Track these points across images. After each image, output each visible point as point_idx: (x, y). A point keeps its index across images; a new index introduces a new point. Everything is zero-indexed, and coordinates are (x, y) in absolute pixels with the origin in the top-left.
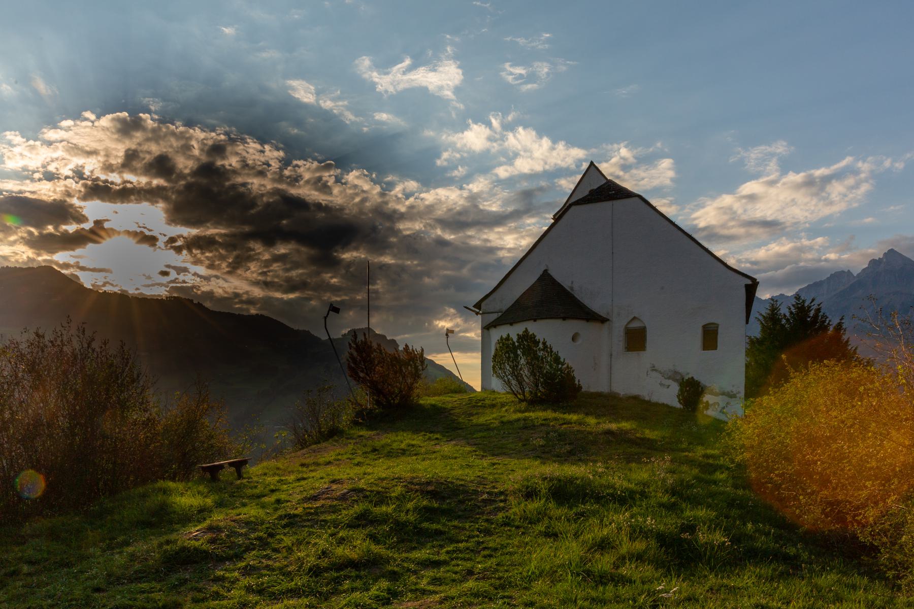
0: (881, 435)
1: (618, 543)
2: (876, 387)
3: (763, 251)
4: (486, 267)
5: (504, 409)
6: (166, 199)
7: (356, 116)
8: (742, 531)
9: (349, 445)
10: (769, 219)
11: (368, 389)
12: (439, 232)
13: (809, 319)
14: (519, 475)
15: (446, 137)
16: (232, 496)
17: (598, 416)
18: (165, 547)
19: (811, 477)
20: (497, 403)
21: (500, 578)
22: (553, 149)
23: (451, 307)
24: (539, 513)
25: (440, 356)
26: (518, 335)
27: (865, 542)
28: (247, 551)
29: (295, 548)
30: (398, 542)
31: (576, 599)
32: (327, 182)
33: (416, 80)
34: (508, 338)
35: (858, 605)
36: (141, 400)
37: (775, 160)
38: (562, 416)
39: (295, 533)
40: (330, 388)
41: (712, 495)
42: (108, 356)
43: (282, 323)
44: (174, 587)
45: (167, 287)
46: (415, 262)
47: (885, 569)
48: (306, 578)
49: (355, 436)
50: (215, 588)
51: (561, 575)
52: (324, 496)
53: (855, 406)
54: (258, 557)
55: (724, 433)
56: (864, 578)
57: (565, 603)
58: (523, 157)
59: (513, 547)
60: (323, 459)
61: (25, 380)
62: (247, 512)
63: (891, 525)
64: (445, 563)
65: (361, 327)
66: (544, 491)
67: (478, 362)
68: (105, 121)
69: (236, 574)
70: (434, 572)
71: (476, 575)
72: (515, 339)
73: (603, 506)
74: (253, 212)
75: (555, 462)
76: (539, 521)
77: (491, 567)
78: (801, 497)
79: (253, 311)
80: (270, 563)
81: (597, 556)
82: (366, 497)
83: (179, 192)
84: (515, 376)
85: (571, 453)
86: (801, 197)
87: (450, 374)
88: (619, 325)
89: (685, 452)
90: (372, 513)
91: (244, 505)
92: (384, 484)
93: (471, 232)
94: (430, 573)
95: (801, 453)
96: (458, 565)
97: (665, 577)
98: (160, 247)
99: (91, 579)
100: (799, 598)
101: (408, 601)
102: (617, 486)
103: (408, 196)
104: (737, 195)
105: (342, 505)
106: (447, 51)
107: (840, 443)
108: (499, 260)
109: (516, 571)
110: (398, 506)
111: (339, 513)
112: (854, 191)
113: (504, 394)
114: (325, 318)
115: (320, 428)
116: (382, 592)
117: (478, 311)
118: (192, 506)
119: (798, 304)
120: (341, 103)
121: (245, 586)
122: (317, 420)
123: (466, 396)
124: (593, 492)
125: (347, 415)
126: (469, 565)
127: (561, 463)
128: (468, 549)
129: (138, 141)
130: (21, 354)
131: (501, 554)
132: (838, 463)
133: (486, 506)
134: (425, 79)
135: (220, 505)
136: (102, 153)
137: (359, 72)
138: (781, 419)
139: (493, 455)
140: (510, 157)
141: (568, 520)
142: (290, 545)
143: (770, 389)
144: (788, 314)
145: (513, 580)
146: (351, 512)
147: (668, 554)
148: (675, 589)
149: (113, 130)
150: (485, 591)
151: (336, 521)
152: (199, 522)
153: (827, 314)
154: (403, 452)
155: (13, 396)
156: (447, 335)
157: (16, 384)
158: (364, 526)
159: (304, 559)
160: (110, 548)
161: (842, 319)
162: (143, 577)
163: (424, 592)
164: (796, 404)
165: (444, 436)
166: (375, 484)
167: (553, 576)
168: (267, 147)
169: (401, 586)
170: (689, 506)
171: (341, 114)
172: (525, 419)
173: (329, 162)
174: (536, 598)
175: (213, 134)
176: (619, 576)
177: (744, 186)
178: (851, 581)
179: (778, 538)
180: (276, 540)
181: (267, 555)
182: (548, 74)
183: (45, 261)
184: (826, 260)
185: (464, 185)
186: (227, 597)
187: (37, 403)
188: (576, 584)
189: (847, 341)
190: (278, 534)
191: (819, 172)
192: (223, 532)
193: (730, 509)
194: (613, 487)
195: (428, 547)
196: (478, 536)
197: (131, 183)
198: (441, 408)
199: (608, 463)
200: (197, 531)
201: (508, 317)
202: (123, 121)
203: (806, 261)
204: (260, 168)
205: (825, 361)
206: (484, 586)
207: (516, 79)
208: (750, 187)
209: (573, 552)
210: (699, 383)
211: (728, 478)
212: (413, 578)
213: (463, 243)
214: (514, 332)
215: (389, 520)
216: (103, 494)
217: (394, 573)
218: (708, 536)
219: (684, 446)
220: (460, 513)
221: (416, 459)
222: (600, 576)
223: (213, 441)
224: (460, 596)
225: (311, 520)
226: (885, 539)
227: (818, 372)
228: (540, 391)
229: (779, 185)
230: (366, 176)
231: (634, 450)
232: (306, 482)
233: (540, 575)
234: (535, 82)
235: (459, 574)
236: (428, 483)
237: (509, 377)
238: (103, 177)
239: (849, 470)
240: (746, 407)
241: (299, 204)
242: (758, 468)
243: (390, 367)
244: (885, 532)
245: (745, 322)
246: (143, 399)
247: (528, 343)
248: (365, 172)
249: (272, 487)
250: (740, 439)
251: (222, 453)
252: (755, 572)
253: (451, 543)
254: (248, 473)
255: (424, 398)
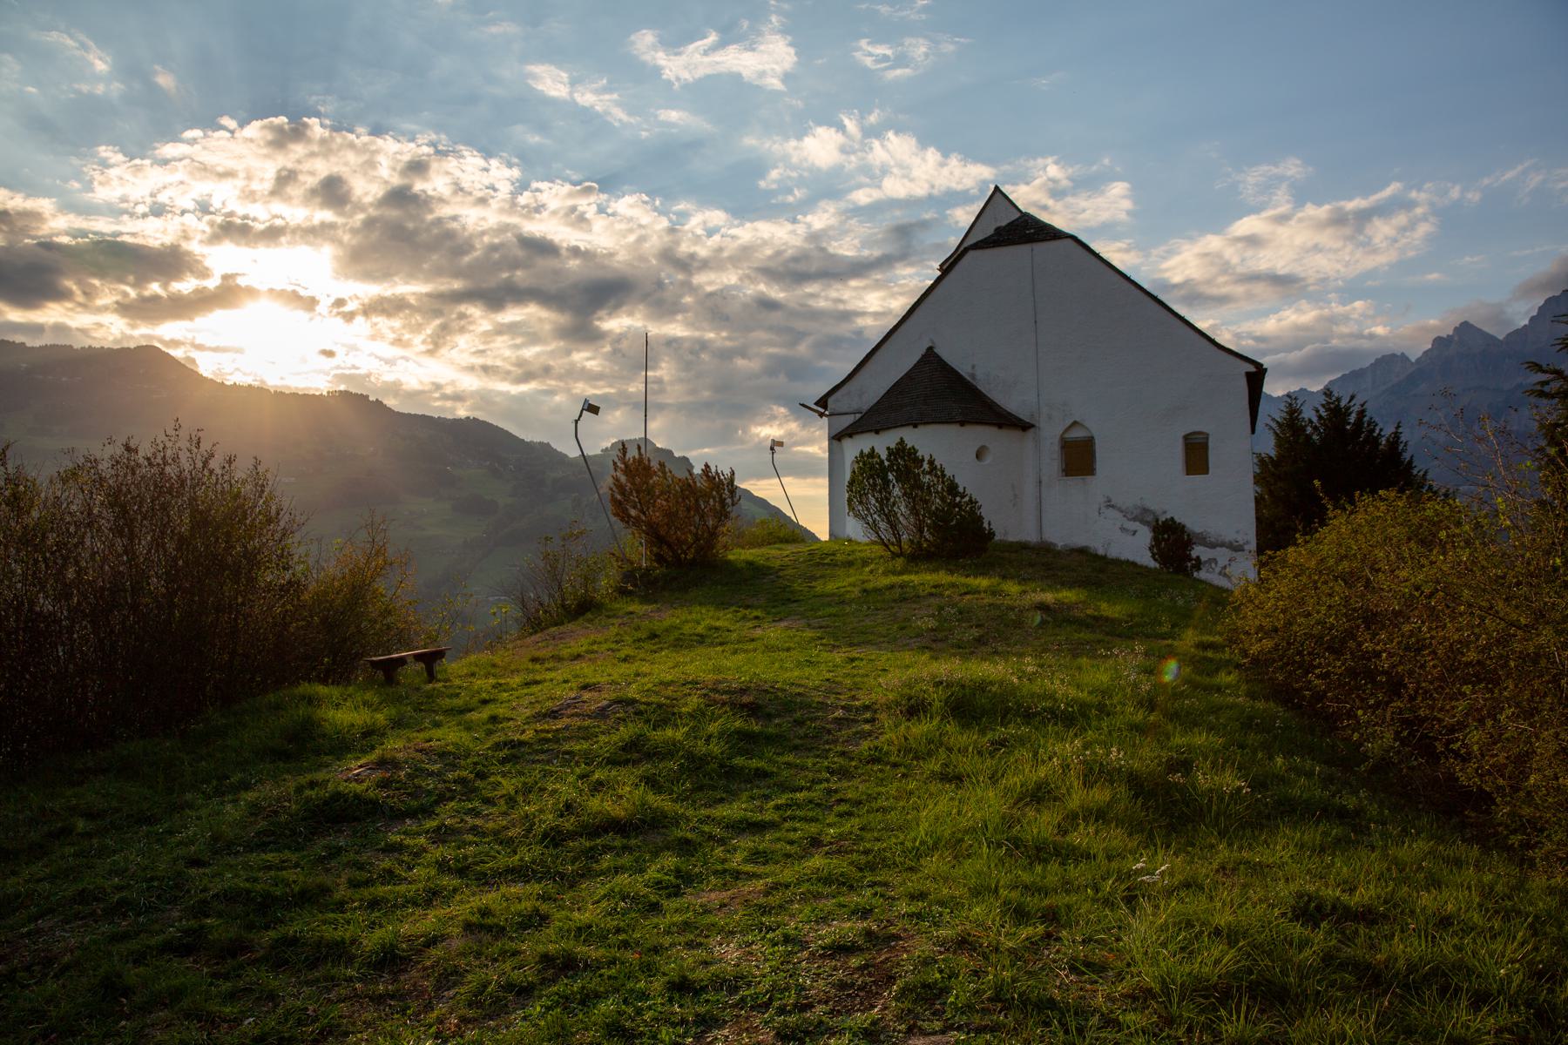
0: (1480, 608)
1: (1064, 791)
2: (1466, 532)
3: (1273, 321)
4: (835, 342)
5: (867, 569)
6: (336, 241)
7: (630, 114)
8: (1267, 768)
9: (611, 628)
10: (1282, 272)
11: (643, 535)
12: (762, 287)
13: (1348, 427)
14: (895, 678)
15: (775, 146)
16: (418, 710)
17: (1023, 581)
18: (308, 792)
19: (1373, 681)
20: (856, 559)
21: (866, 852)
22: (942, 165)
23: (780, 405)
24: (930, 742)
25: (763, 483)
26: (888, 448)
27: (1469, 786)
28: (442, 802)
29: (520, 799)
30: (693, 791)
31: (996, 887)
32: (585, 213)
33: (723, 62)
34: (872, 454)
35: (1467, 892)
36: (279, 552)
37: (1284, 186)
38: (963, 580)
39: (521, 773)
40: (581, 533)
41: (1216, 710)
42: (233, 482)
43: (507, 432)
44: (321, 860)
45: (328, 374)
46: (724, 334)
47: (1505, 832)
48: (537, 850)
49: (620, 614)
50: (387, 863)
51: (971, 846)
52: (569, 711)
53: (1435, 563)
54: (458, 812)
55: (1228, 608)
56: (1472, 847)
57: (979, 893)
58: (895, 176)
59: (887, 799)
60: (569, 650)
61: (103, 518)
62: (441, 737)
63: (1507, 758)
64: (773, 825)
65: (633, 438)
66: (937, 704)
67: (824, 492)
68: (254, 129)
69: (422, 840)
70: (754, 842)
71: (826, 846)
72: (884, 456)
73: (1036, 729)
74: (467, 259)
75: (955, 655)
76: (930, 754)
77: (851, 833)
78: (1360, 712)
79: (462, 413)
80: (478, 822)
81: (1031, 813)
82: (639, 713)
83: (354, 231)
84: (886, 515)
85: (980, 641)
86: (1326, 238)
87: (777, 512)
88: (1051, 433)
89: (1167, 639)
90: (649, 740)
91: (437, 725)
92: (669, 692)
93: (811, 288)
94: (747, 843)
95: (1355, 640)
96: (795, 830)
97: (1145, 848)
98: (320, 314)
99: (186, 845)
100: (1368, 882)
101: (710, 890)
102: (1059, 695)
103: (710, 232)
104: (1228, 237)
105: (599, 727)
106: (771, 22)
107: (1415, 623)
108: (859, 332)
109: (894, 840)
110: (693, 729)
111: (595, 739)
112: (1408, 234)
113: (867, 544)
114: (576, 422)
115: (563, 600)
116: (666, 874)
117: (822, 410)
118: (353, 725)
119: (1328, 403)
120: (607, 97)
121: (437, 862)
122: (560, 587)
123: (803, 548)
124: (1020, 706)
125: (607, 576)
126: (813, 829)
127: (965, 658)
128: (810, 802)
129: (297, 156)
130: (100, 478)
131: (868, 811)
132: (1415, 656)
133: (840, 730)
134: (736, 62)
135: (398, 724)
136: (242, 175)
137: (635, 52)
138: (1319, 585)
139: (851, 645)
140: (875, 175)
141: (979, 752)
142: (513, 793)
143: (1297, 535)
144: (1315, 419)
145: (888, 855)
146: (615, 738)
147: (1147, 809)
148: (1163, 868)
149: (262, 143)
150: (842, 875)
151: (589, 754)
152: (364, 752)
153: (1376, 419)
154: (701, 639)
155: (82, 543)
156: (772, 449)
157: (88, 524)
158: (635, 763)
159: (534, 817)
160: (218, 792)
161: (1398, 427)
162: (270, 843)
163: (737, 875)
164: (1341, 560)
165: (768, 613)
166: (655, 692)
167: (956, 847)
168: (494, 163)
169: (699, 864)
170: (1179, 728)
171: (607, 113)
172: (902, 586)
173: (587, 184)
174: (929, 885)
175: (412, 145)
176: (1068, 846)
177: (1239, 223)
178: (1452, 854)
179: (1327, 781)
180: (489, 784)
181: (473, 809)
182: (927, 55)
183: (143, 336)
184: (1372, 336)
185: (799, 217)
186: (406, 879)
187: (120, 555)
188: (997, 861)
189: (1410, 462)
190: (493, 773)
191: (1351, 205)
192: (402, 769)
193: (1246, 733)
194: (1052, 697)
195: (744, 799)
196: (827, 781)
197: (283, 218)
198: (764, 566)
199: (1041, 658)
200: (361, 767)
201: (870, 421)
202: (279, 130)
203: (1342, 336)
204: (480, 194)
205: (1381, 492)
206: (839, 865)
207: (877, 61)
208: (1246, 225)
209: (989, 806)
210: (1184, 526)
211: (1238, 682)
212: (719, 851)
213: (802, 305)
214: (881, 444)
215: (678, 752)
216: (212, 705)
217: (687, 842)
218: (1212, 778)
219: (1165, 629)
220: (798, 742)
221: (723, 651)
222: (1036, 847)
223: (390, 619)
224: (799, 883)
225: (548, 751)
226: (1501, 782)
227: (1371, 509)
228: (926, 540)
229: (1292, 223)
230: (645, 203)
231: (1084, 635)
232: (540, 687)
233: (935, 847)
234: (907, 66)
235: (796, 845)
236: (743, 691)
237: (875, 516)
238: (241, 211)
239: (1434, 667)
240: (1262, 565)
241: (541, 248)
242: (1287, 664)
243: (680, 500)
244: (1500, 769)
245: (1250, 431)
246: (283, 549)
247: (905, 461)
248: (646, 198)
249: (484, 695)
250: (1256, 617)
251: (404, 641)
252: (1293, 838)
253: (783, 792)
254: (445, 671)
255: (735, 551)
